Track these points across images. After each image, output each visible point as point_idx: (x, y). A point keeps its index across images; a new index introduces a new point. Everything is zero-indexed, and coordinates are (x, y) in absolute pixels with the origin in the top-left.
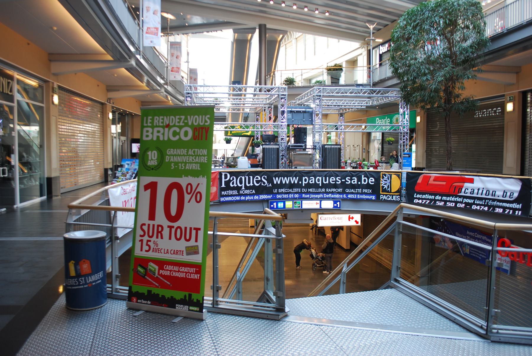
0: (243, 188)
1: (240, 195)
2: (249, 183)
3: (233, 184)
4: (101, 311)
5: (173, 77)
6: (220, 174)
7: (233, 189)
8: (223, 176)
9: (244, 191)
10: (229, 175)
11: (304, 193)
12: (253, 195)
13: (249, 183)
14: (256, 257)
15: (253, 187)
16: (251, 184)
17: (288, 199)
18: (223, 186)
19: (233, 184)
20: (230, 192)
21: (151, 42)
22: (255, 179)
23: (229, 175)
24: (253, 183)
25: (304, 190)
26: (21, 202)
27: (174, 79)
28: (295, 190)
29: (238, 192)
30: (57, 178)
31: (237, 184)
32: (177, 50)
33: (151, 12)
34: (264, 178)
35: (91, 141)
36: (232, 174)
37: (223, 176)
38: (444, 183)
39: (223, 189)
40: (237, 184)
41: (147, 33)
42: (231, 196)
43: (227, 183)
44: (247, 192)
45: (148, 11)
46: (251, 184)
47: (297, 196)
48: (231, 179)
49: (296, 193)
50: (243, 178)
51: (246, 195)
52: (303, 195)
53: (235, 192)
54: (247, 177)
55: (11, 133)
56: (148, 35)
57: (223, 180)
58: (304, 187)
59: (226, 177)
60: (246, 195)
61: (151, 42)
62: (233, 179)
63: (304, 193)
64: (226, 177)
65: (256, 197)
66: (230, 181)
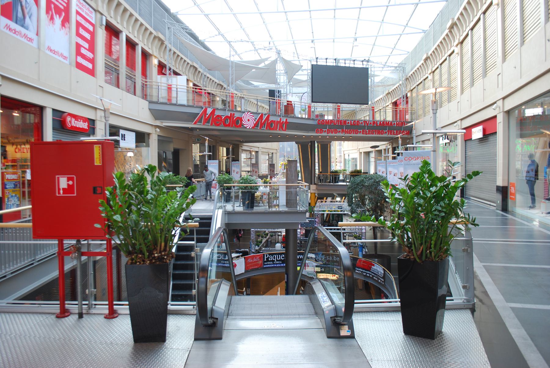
1: (274, 264)
4: (449, 67)
6: (264, 255)
7: (271, 261)
9: (276, 262)
12: (281, 264)
14: (54, 129)
15: (281, 260)
20: (269, 263)
30: (517, 137)
35: (18, 351)
36: (269, 254)
38: (97, 162)
39: (266, 262)
43: (267, 259)
44: (278, 262)
51: (277, 264)
53: (271, 263)
55: (446, 220)
59: (267, 256)
60: (277, 264)
64: (267, 256)
65: (282, 265)
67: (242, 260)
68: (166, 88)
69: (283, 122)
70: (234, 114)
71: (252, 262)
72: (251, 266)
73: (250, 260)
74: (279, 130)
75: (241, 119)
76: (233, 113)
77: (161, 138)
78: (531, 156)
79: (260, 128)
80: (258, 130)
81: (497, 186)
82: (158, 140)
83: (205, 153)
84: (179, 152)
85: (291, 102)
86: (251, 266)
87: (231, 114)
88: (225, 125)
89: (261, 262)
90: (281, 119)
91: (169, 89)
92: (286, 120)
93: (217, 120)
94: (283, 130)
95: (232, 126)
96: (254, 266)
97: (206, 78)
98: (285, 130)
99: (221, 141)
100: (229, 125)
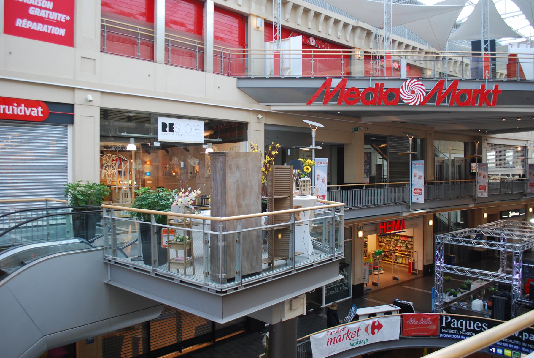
0: (464, 330)
2: (470, 326)
3: (454, 325)
5: (480, 194)
6: (441, 316)
7: (454, 329)
8: (444, 318)
10: (450, 318)
11: (524, 347)
13: (470, 326)
16: (472, 328)
17: (508, 348)
18: (444, 325)
19: (454, 325)
20: (451, 331)
21: (417, 199)
22: (475, 325)
23: (450, 318)
24: (474, 327)
25: (524, 344)
26: (326, 304)
27: (482, 196)
28: (515, 342)
29: (459, 332)
31: (457, 325)
32: (484, 171)
33: (417, 177)
34: (485, 325)
36: (452, 317)
37: (444, 318)
39: (444, 328)
40: (457, 325)
41: (414, 193)
42: (452, 334)
45: (415, 176)
46: (472, 328)
47: (516, 347)
48: (452, 321)
49: (517, 345)
50: (464, 322)
52: (523, 349)
53: (456, 332)
54: (468, 322)
56: (415, 194)
57: (444, 321)
58: (524, 342)
61: (417, 199)
62: (454, 321)
63: (524, 347)
66: (450, 322)
67: (396, 319)
68: (272, 56)
69: (488, 91)
70: (383, 85)
71: (417, 325)
72: (414, 331)
73: (411, 321)
74: (480, 105)
75: (398, 91)
76: (380, 82)
77: (269, 128)
78: (263, 184)
79: (438, 104)
80: (431, 107)
81: (495, 40)
82: (266, 132)
83: (311, 147)
84: (343, 148)
85: (515, 55)
86: (414, 331)
87: (377, 85)
88: (366, 103)
89: (434, 327)
90: (483, 87)
91: (277, 57)
92: (497, 87)
93: (352, 95)
94: (489, 105)
95: (379, 104)
96: (420, 331)
97: (410, 50)
98: (494, 105)
99: (436, 132)
100: (372, 103)
